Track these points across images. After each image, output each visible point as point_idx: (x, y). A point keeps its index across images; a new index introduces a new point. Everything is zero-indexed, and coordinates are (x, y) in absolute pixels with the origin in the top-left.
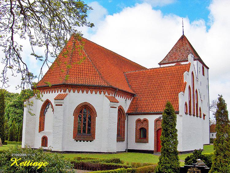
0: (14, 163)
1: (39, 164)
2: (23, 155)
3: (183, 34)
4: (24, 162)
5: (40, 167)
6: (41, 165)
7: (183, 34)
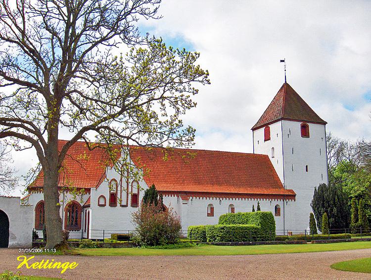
0: (23, 263)
1: (63, 265)
2: (37, 251)
3: (286, 82)
4: (38, 263)
5: (65, 270)
6: (66, 267)
7: (286, 82)
